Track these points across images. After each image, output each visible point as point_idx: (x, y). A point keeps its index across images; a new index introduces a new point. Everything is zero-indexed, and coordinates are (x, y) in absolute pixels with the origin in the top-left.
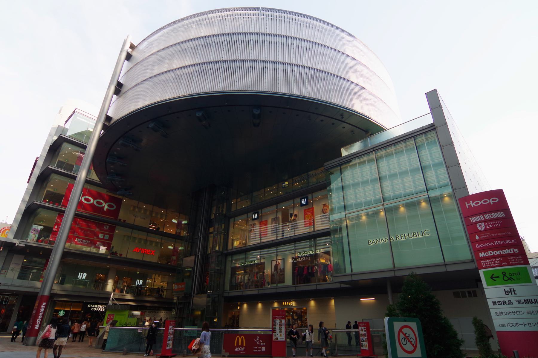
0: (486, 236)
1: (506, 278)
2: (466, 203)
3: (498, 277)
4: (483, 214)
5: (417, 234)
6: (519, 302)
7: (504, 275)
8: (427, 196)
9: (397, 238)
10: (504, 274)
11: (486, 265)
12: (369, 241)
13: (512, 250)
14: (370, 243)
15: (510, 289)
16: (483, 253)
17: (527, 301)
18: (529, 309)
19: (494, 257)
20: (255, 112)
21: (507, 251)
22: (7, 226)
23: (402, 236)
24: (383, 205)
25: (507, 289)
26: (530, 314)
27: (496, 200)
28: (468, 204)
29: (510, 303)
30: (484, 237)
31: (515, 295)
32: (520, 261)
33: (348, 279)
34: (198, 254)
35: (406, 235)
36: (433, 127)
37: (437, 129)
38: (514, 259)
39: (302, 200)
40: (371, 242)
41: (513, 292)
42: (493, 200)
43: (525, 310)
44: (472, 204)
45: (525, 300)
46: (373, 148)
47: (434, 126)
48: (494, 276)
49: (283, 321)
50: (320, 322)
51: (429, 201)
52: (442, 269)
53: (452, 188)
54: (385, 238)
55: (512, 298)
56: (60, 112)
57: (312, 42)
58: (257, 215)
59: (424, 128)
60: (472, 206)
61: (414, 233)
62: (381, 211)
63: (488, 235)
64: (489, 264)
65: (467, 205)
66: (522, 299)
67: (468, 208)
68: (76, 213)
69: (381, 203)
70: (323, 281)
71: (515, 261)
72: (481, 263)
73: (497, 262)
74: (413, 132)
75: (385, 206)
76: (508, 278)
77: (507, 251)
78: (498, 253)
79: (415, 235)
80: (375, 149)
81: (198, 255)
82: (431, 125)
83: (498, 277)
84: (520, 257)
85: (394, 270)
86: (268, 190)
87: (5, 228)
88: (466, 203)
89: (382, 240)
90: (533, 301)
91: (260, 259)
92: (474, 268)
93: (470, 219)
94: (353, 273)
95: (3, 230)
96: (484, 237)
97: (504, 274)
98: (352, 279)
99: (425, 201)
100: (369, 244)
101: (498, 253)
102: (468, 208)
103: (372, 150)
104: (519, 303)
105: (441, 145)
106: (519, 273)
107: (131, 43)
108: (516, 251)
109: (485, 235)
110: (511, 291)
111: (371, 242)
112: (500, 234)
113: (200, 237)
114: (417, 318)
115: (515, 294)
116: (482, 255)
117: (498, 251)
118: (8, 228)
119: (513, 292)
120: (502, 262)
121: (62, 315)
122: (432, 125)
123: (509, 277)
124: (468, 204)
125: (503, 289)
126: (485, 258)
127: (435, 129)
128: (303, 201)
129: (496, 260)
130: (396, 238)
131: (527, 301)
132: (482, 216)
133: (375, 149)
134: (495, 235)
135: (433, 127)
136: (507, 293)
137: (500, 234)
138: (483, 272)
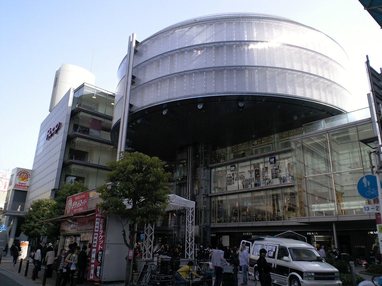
20: (240, 105)
22: (22, 171)
34: (188, 195)
36: (371, 121)
39: (271, 159)
49: (234, 39)
50: (125, 259)
56: (57, 78)
57: (288, 45)
58: (234, 168)
70: (273, 221)
80: (328, 131)
81: (188, 196)
82: (369, 119)
86: (243, 147)
87: (21, 171)
91: (226, 171)
95: (20, 173)
107: (136, 40)
113: (189, 183)
114: (222, 243)
118: (23, 172)
128: (271, 160)
135: (371, 121)
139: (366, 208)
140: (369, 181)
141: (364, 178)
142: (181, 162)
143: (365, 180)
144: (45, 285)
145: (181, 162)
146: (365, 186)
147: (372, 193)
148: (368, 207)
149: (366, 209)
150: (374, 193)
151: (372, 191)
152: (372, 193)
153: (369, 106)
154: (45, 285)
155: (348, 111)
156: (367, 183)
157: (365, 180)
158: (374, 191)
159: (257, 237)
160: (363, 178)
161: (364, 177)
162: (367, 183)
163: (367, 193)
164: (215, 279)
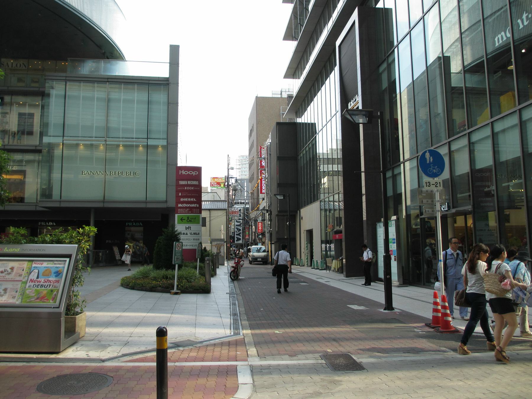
0: (185, 195)
1: (188, 221)
2: (180, 171)
3: (185, 219)
4: (187, 180)
5: (129, 173)
6: (191, 234)
7: (188, 219)
8: (146, 144)
9: (111, 174)
10: (188, 218)
11: (180, 211)
12: (83, 172)
13: (196, 205)
14: (83, 174)
15: (189, 227)
16: (181, 204)
17: (194, 234)
18: (194, 238)
19: (186, 208)
21: (193, 205)
23: (116, 172)
24: (106, 141)
25: (187, 226)
26: (194, 240)
27: (196, 173)
28: (181, 171)
29: (187, 234)
30: (184, 195)
31: (190, 230)
32: (198, 212)
33: (57, 205)
35: (120, 172)
36: (167, 82)
37: (170, 85)
38: (195, 210)
40: (85, 173)
41: (189, 229)
42: (195, 173)
43: (192, 238)
44: (183, 172)
45: (194, 233)
46: (108, 78)
47: (168, 81)
48: (183, 219)
51: (147, 147)
52: (143, 206)
53: (167, 142)
54: (100, 172)
55: (188, 232)
59: (160, 79)
60: (183, 174)
61: (127, 172)
62: (101, 145)
63: (185, 194)
64: (180, 211)
65: (180, 172)
66: (193, 232)
67: (180, 174)
68: (43, 189)
69: (104, 139)
71: (195, 211)
72: (178, 210)
73: (186, 211)
74: (149, 79)
75: (107, 143)
76: (190, 220)
77: (193, 205)
78: (189, 205)
79: (127, 174)
82: (166, 79)
83: (185, 219)
84: (198, 209)
85: (104, 201)
88: (180, 171)
89: (97, 173)
90: (198, 234)
92: (165, 207)
93: (180, 182)
94: (61, 200)
96: (184, 195)
97: (188, 218)
98: (60, 205)
99: (143, 146)
100: (82, 174)
101: (189, 205)
102: (180, 174)
103: (106, 80)
104: (191, 234)
105: (169, 102)
106: (195, 218)
108: (198, 206)
109: (185, 194)
110: (189, 228)
111: (85, 173)
112: (193, 195)
115: (190, 229)
116: (180, 205)
117: (189, 205)
119: (189, 229)
120: (189, 211)
121: (175, 237)
122: (166, 79)
123: (190, 220)
124: (181, 171)
125: (185, 226)
126: (180, 208)
127: (168, 84)
129: (186, 210)
130: (111, 173)
131: (194, 234)
132: (186, 182)
133: (109, 80)
134: (190, 195)
135: (167, 82)
136: (186, 228)
137: (193, 195)
138: (178, 215)
139: (427, 183)
140: (431, 157)
141: (427, 152)
142: (348, 306)
143: (427, 155)
144: (171, 46)
145: (348, 306)
146: (428, 162)
147: (434, 171)
148: (436, 182)
149: (428, 184)
150: (436, 172)
151: (434, 169)
152: (434, 171)
153: (169, 62)
154: (171, 46)
155: (127, 60)
156: (430, 159)
157: (427, 155)
158: (436, 169)
159: (397, 221)
160: (426, 152)
161: (428, 151)
162: (430, 159)
163: (429, 171)
164: (186, 200)
